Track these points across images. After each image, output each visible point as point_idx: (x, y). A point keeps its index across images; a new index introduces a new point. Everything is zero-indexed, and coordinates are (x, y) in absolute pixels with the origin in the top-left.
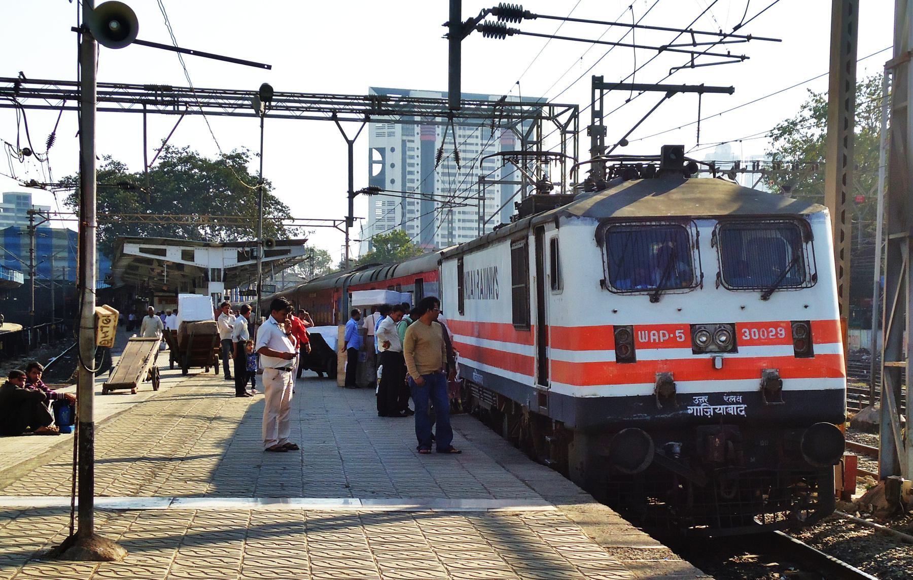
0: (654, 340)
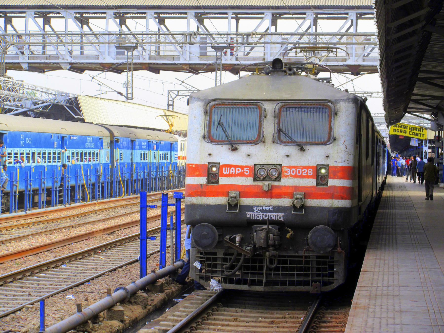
0: (232, 173)
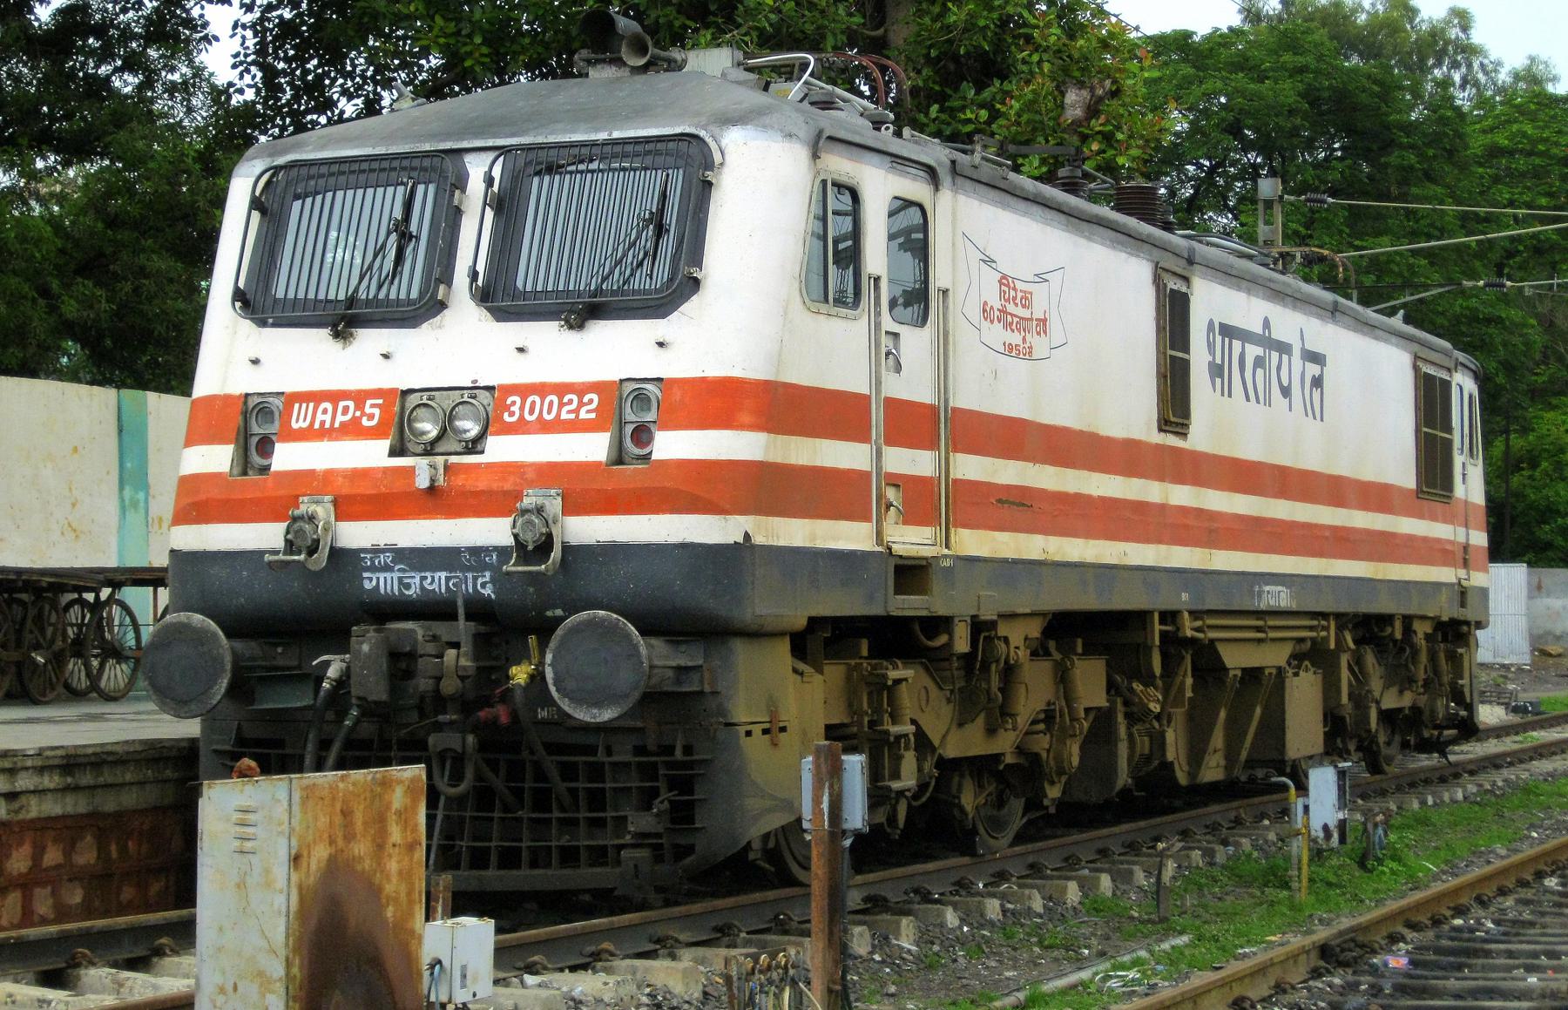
0: (323, 423)
